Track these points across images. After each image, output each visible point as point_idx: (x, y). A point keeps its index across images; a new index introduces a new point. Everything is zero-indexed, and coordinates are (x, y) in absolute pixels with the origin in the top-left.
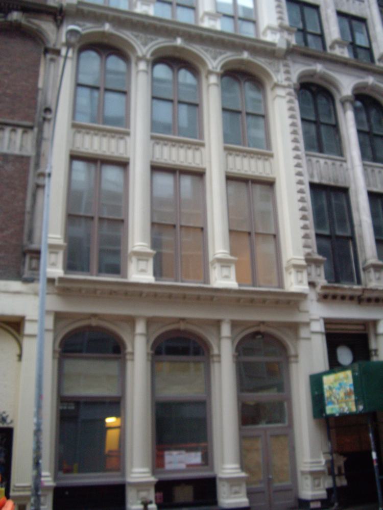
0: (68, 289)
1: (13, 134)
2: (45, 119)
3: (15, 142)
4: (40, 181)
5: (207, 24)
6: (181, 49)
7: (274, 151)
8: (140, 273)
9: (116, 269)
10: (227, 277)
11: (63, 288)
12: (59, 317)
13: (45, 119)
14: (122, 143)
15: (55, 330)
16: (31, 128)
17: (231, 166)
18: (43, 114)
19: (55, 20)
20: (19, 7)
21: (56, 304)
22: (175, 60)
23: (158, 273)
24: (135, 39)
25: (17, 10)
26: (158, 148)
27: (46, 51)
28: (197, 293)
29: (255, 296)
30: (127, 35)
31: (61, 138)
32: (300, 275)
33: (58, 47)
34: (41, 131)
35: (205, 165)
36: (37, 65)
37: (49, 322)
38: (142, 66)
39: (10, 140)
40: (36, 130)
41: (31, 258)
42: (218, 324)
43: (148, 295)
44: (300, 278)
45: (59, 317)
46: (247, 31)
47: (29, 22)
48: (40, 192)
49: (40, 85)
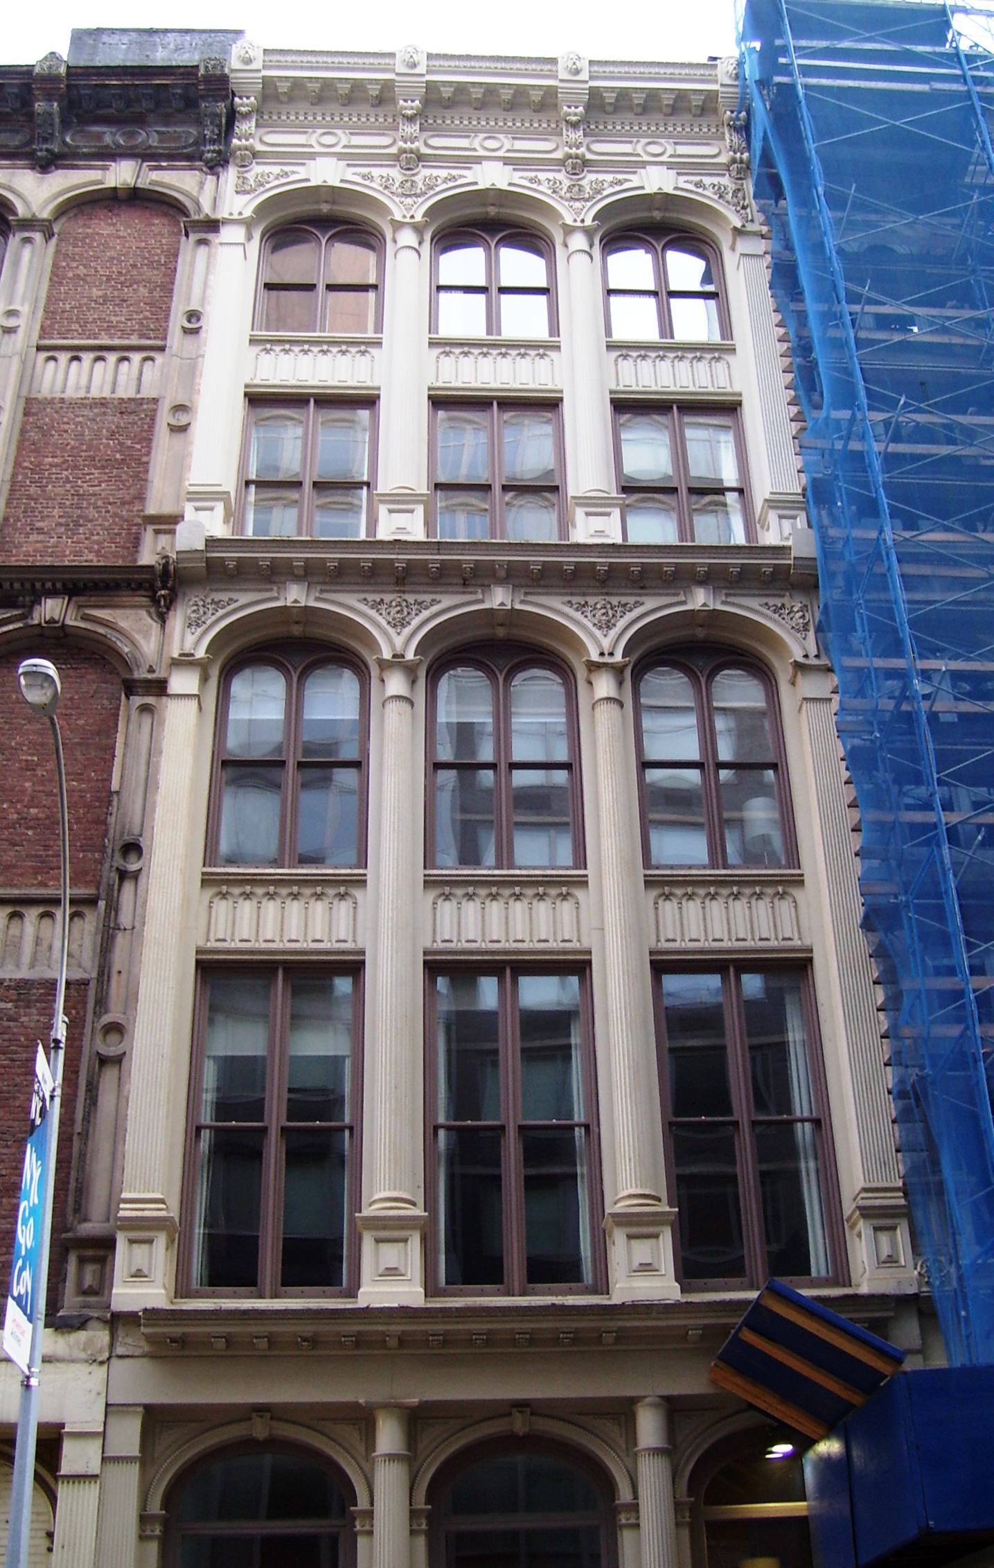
0: (182, 1342)
1: (46, 922)
2: (123, 875)
3: (50, 948)
4: (110, 1048)
5: (585, 530)
6: (714, 616)
7: (806, 869)
8: (391, 1278)
9: (555, 1267)
10: (646, 1268)
11: (170, 1339)
12: (156, 1419)
13: (123, 875)
14: (785, 907)
15: (147, 1458)
16: (92, 902)
17: (669, 930)
18: (118, 861)
19: (155, 601)
20: (59, 585)
21: (141, 1382)
22: (693, 651)
23: (688, 1272)
24: (578, 616)
25: (53, 593)
26: (447, 909)
27: (131, 687)
28: (308, 1329)
29: (323, 1328)
30: (352, 606)
31: (173, 918)
32: (884, 1238)
33: (159, 674)
34: (113, 907)
35: (589, 941)
36: (108, 726)
37: (128, 1436)
38: (604, 686)
39: (38, 941)
40: (102, 904)
41: (82, 1261)
42: (622, 1412)
43: (403, 1341)
44: (885, 1251)
45: (156, 1419)
46: (532, 525)
47: (85, 618)
48: (109, 1076)
49: (115, 786)
